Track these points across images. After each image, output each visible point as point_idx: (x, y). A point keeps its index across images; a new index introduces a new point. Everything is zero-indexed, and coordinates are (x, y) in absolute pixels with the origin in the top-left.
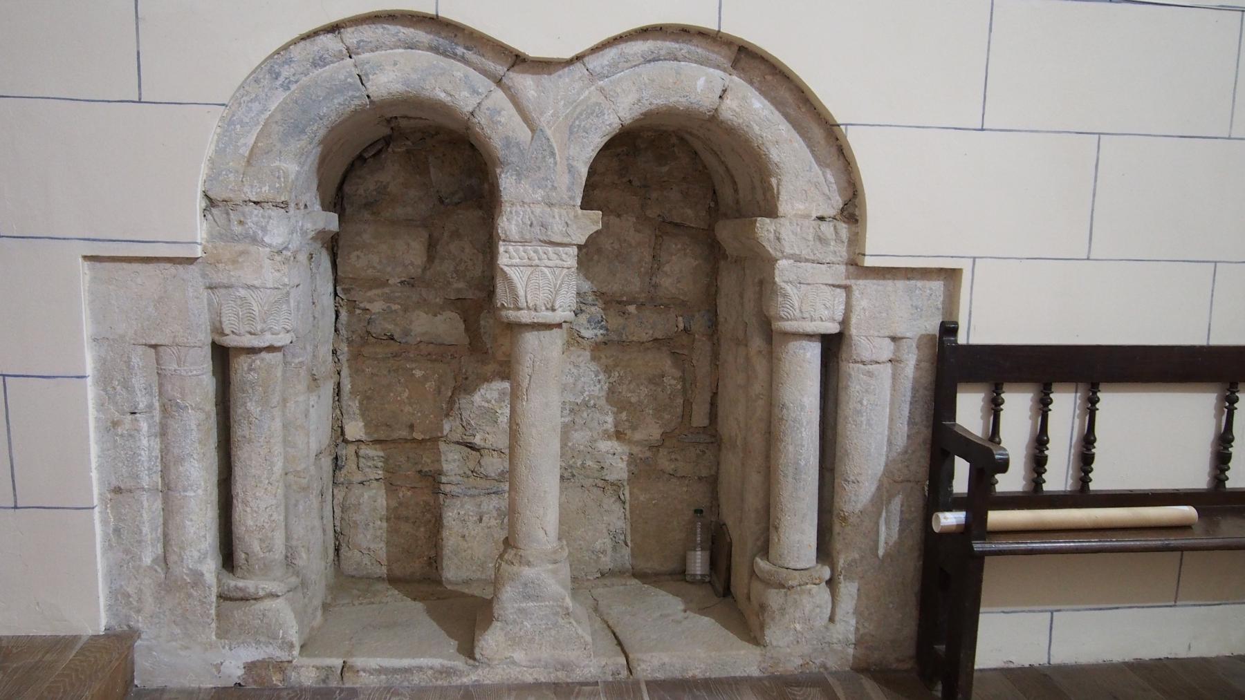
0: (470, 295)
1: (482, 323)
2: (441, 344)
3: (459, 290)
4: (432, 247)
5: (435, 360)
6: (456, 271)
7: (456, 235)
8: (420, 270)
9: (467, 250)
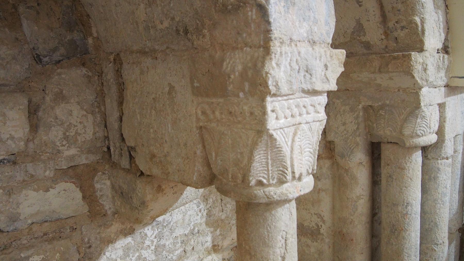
0: (83, 160)
1: (98, 186)
2: (57, 220)
3: (72, 158)
4: (33, 112)
5: (54, 238)
6: (66, 138)
7: (60, 97)
8: (22, 143)
9: (75, 113)
